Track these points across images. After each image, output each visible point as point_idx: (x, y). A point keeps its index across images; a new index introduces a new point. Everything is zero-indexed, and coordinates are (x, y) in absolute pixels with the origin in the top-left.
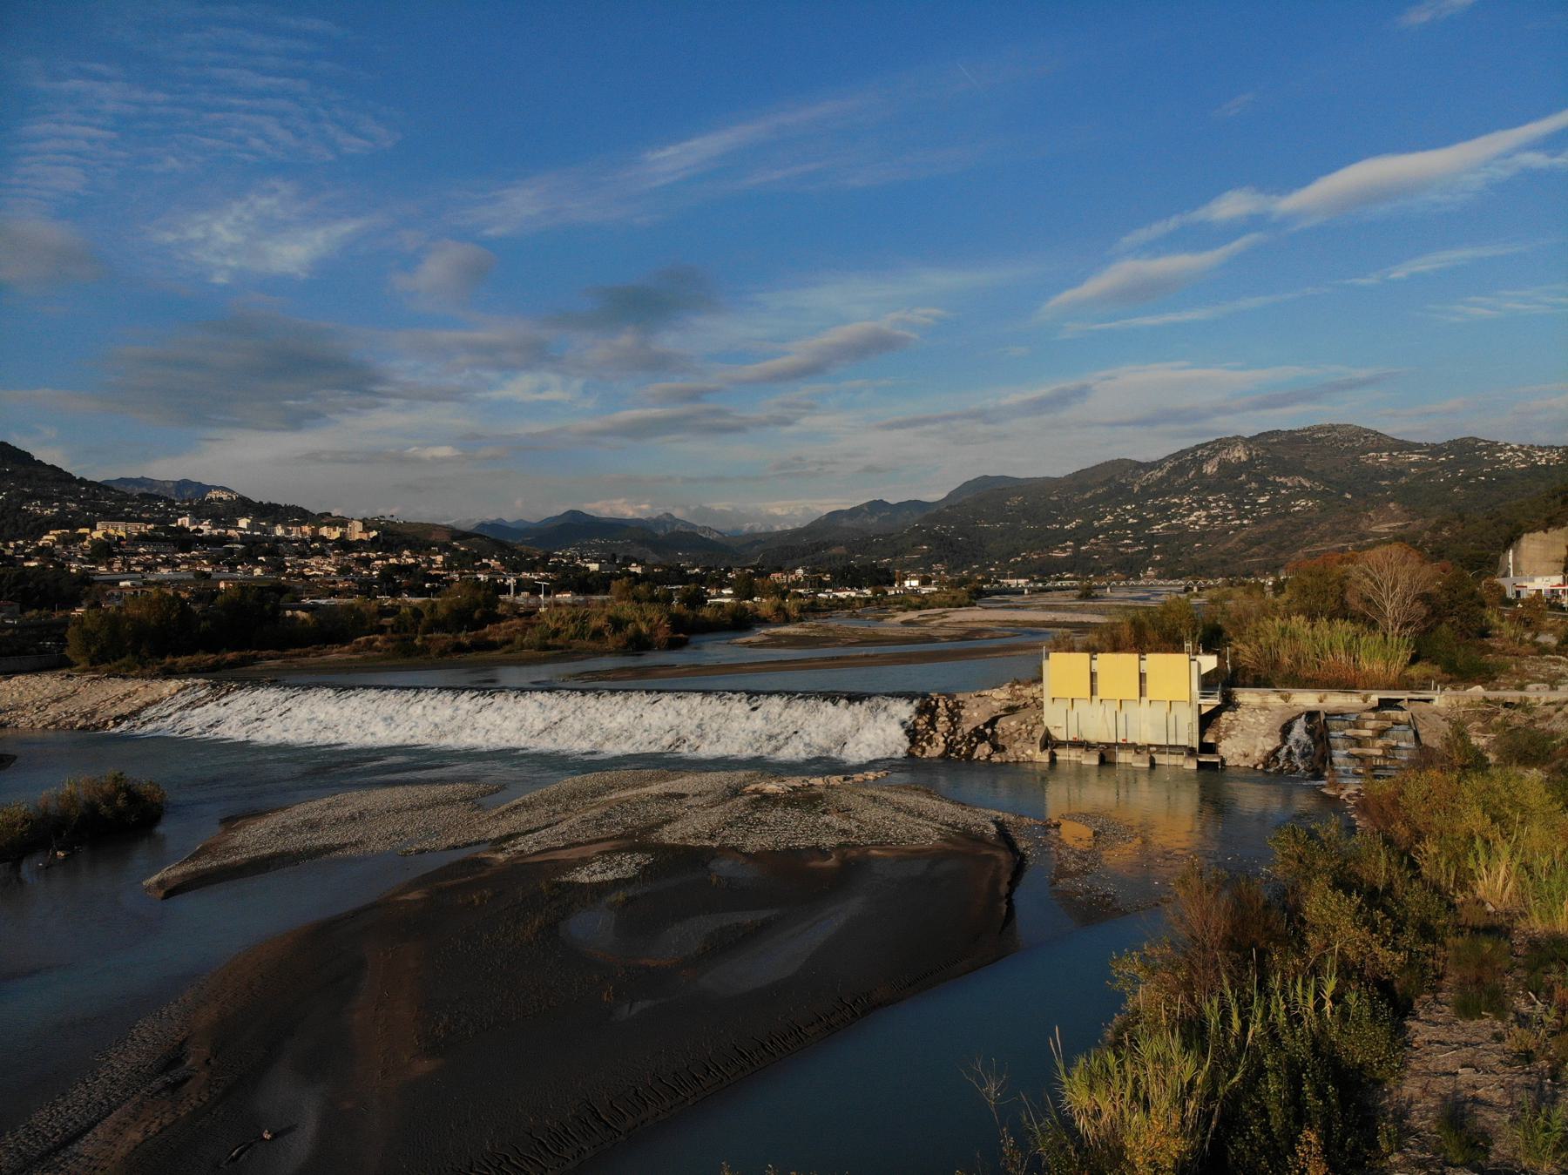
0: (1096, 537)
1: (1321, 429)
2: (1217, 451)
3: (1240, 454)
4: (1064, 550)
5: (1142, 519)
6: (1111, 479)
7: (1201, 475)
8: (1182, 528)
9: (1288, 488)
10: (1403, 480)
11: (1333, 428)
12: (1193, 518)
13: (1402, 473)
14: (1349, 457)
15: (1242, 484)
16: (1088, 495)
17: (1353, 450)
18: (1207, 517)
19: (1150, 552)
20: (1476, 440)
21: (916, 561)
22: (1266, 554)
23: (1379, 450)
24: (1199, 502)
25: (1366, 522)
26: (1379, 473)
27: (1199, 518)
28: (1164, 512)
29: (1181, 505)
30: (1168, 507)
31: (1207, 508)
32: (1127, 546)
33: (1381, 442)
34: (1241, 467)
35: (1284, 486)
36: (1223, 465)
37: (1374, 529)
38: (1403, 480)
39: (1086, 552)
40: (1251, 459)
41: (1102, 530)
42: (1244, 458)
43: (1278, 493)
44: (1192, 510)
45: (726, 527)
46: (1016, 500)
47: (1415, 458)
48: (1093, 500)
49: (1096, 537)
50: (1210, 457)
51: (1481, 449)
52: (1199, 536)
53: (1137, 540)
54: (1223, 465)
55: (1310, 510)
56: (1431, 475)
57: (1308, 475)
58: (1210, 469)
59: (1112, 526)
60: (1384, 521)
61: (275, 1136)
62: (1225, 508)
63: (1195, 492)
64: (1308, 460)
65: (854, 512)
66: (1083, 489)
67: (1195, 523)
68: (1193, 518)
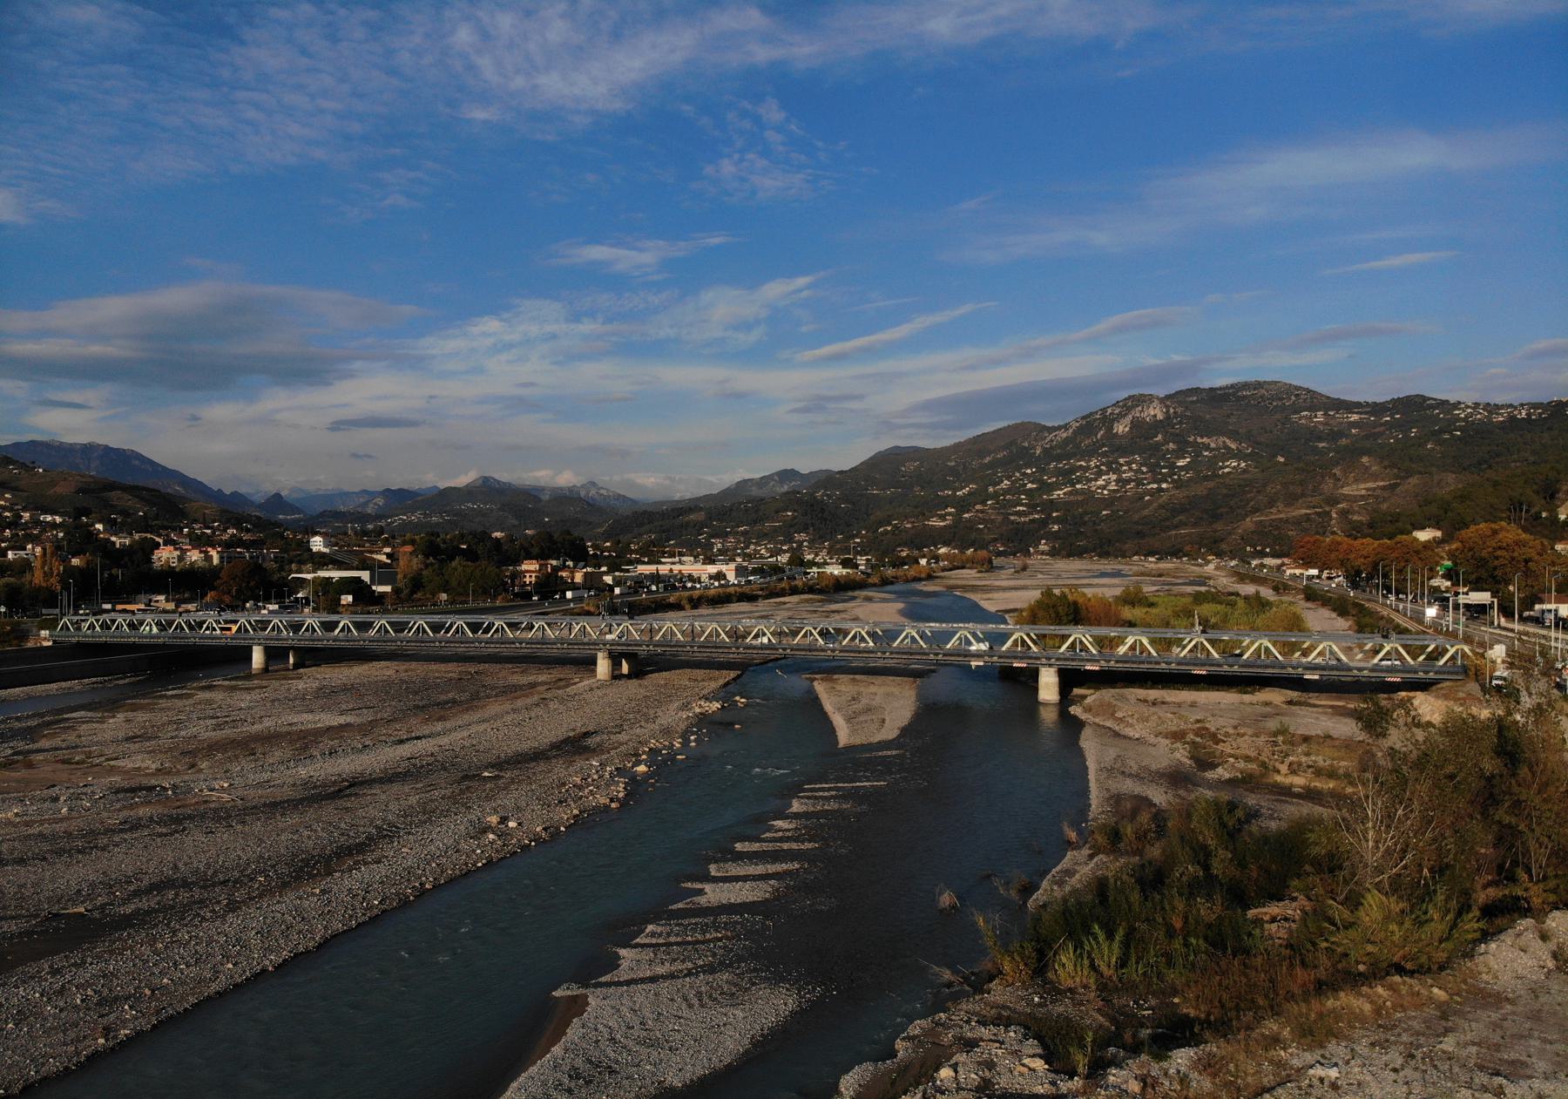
0: (984, 503)
1: (1246, 386)
2: (1129, 409)
3: (1155, 412)
4: (943, 517)
5: (1042, 484)
6: (1013, 443)
7: (1111, 436)
8: (1089, 494)
9: (1211, 450)
10: (1344, 441)
11: (1258, 385)
12: (1100, 482)
13: (1340, 434)
14: (1278, 416)
15: (1158, 446)
16: (987, 460)
17: (1284, 408)
18: (1117, 481)
19: (1044, 523)
20: (1425, 399)
21: (775, 530)
22: (1195, 525)
23: (1313, 408)
24: (1109, 465)
25: (1330, 482)
26: (1314, 434)
27: (1108, 482)
28: (1067, 476)
29: (1088, 468)
30: (1073, 470)
31: (1117, 471)
32: (1019, 514)
33: (1315, 401)
34: (1156, 425)
35: (1207, 448)
36: (1137, 424)
37: (1346, 490)
38: (1344, 441)
39: (969, 520)
40: (1168, 417)
41: (995, 496)
42: (1160, 417)
43: (1199, 454)
44: (1099, 474)
45: (658, 497)
46: (912, 466)
47: (1355, 417)
48: (992, 465)
49: (984, 503)
50: (1122, 415)
51: (1432, 407)
52: (1109, 502)
53: (1032, 507)
54: (1137, 424)
55: (1245, 471)
56: (1375, 436)
57: (1233, 435)
58: (1121, 428)
59: (1006, 492)
60: (1356, 481)
61: (732, 724)
62: (1138, 471)
63: (1104, 454)
64: (1233, 420)
65: (764, 481)
66: (981, 454)
67: (1104, 488)
68: (1100, 482)
